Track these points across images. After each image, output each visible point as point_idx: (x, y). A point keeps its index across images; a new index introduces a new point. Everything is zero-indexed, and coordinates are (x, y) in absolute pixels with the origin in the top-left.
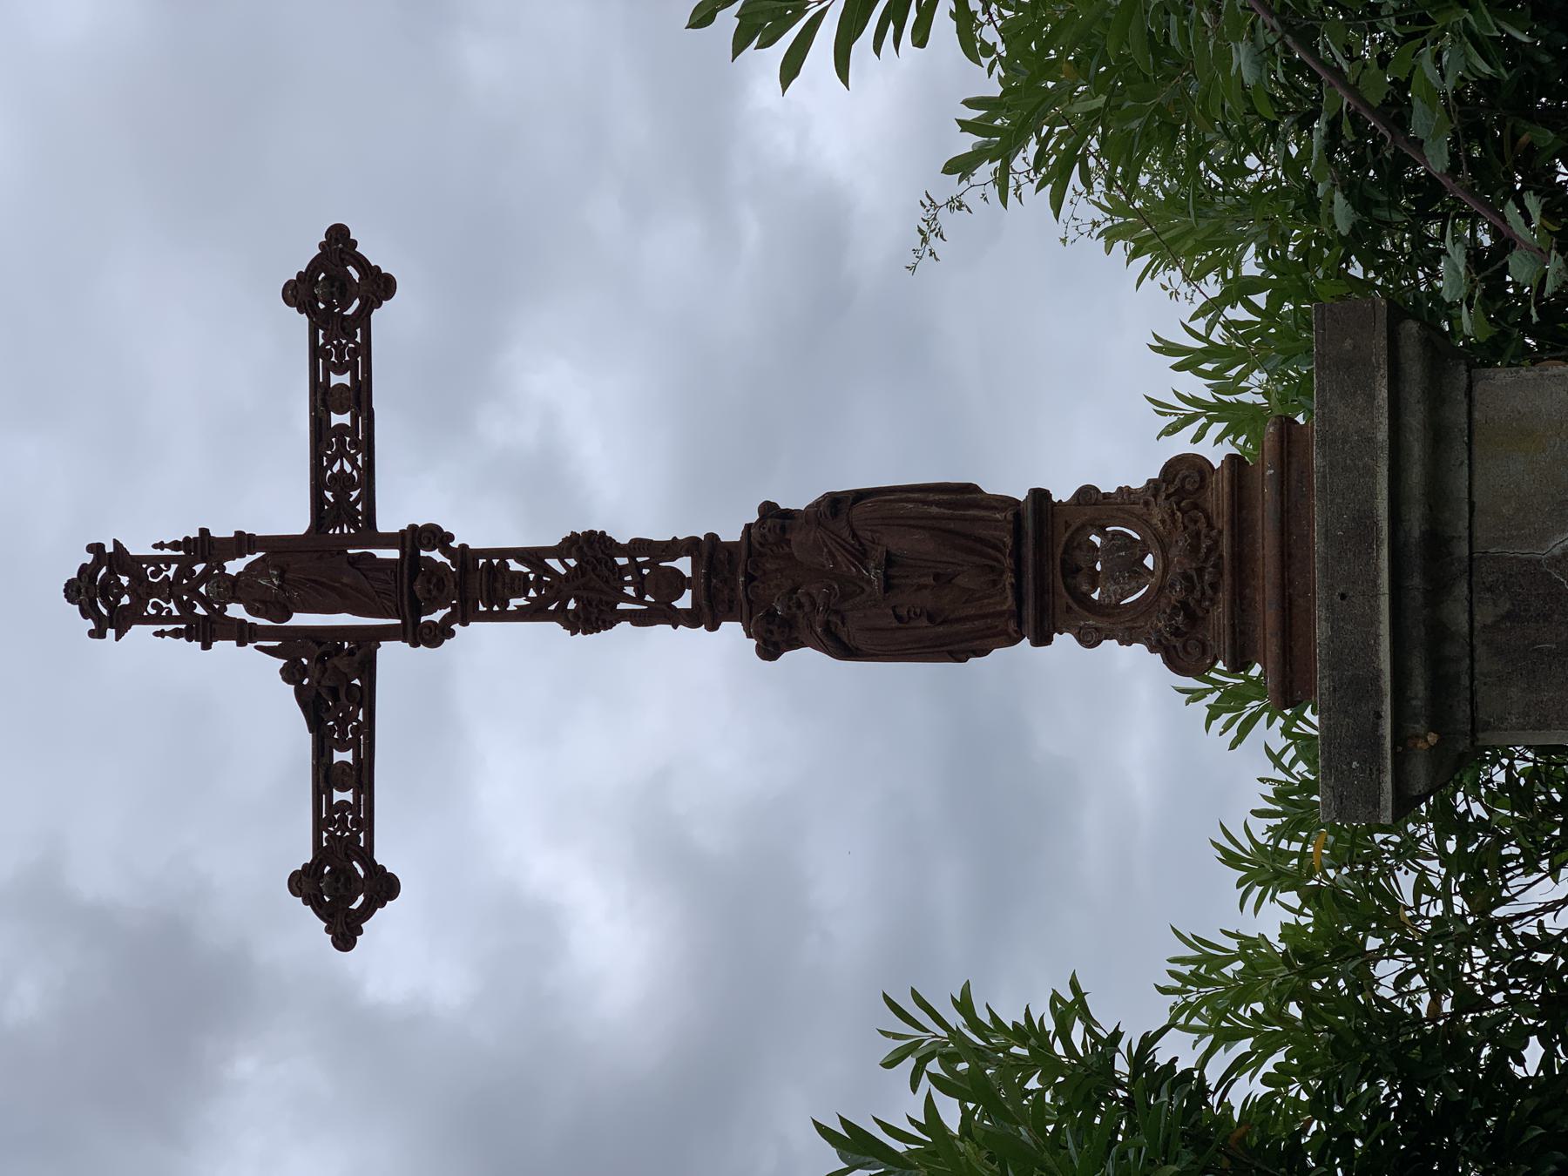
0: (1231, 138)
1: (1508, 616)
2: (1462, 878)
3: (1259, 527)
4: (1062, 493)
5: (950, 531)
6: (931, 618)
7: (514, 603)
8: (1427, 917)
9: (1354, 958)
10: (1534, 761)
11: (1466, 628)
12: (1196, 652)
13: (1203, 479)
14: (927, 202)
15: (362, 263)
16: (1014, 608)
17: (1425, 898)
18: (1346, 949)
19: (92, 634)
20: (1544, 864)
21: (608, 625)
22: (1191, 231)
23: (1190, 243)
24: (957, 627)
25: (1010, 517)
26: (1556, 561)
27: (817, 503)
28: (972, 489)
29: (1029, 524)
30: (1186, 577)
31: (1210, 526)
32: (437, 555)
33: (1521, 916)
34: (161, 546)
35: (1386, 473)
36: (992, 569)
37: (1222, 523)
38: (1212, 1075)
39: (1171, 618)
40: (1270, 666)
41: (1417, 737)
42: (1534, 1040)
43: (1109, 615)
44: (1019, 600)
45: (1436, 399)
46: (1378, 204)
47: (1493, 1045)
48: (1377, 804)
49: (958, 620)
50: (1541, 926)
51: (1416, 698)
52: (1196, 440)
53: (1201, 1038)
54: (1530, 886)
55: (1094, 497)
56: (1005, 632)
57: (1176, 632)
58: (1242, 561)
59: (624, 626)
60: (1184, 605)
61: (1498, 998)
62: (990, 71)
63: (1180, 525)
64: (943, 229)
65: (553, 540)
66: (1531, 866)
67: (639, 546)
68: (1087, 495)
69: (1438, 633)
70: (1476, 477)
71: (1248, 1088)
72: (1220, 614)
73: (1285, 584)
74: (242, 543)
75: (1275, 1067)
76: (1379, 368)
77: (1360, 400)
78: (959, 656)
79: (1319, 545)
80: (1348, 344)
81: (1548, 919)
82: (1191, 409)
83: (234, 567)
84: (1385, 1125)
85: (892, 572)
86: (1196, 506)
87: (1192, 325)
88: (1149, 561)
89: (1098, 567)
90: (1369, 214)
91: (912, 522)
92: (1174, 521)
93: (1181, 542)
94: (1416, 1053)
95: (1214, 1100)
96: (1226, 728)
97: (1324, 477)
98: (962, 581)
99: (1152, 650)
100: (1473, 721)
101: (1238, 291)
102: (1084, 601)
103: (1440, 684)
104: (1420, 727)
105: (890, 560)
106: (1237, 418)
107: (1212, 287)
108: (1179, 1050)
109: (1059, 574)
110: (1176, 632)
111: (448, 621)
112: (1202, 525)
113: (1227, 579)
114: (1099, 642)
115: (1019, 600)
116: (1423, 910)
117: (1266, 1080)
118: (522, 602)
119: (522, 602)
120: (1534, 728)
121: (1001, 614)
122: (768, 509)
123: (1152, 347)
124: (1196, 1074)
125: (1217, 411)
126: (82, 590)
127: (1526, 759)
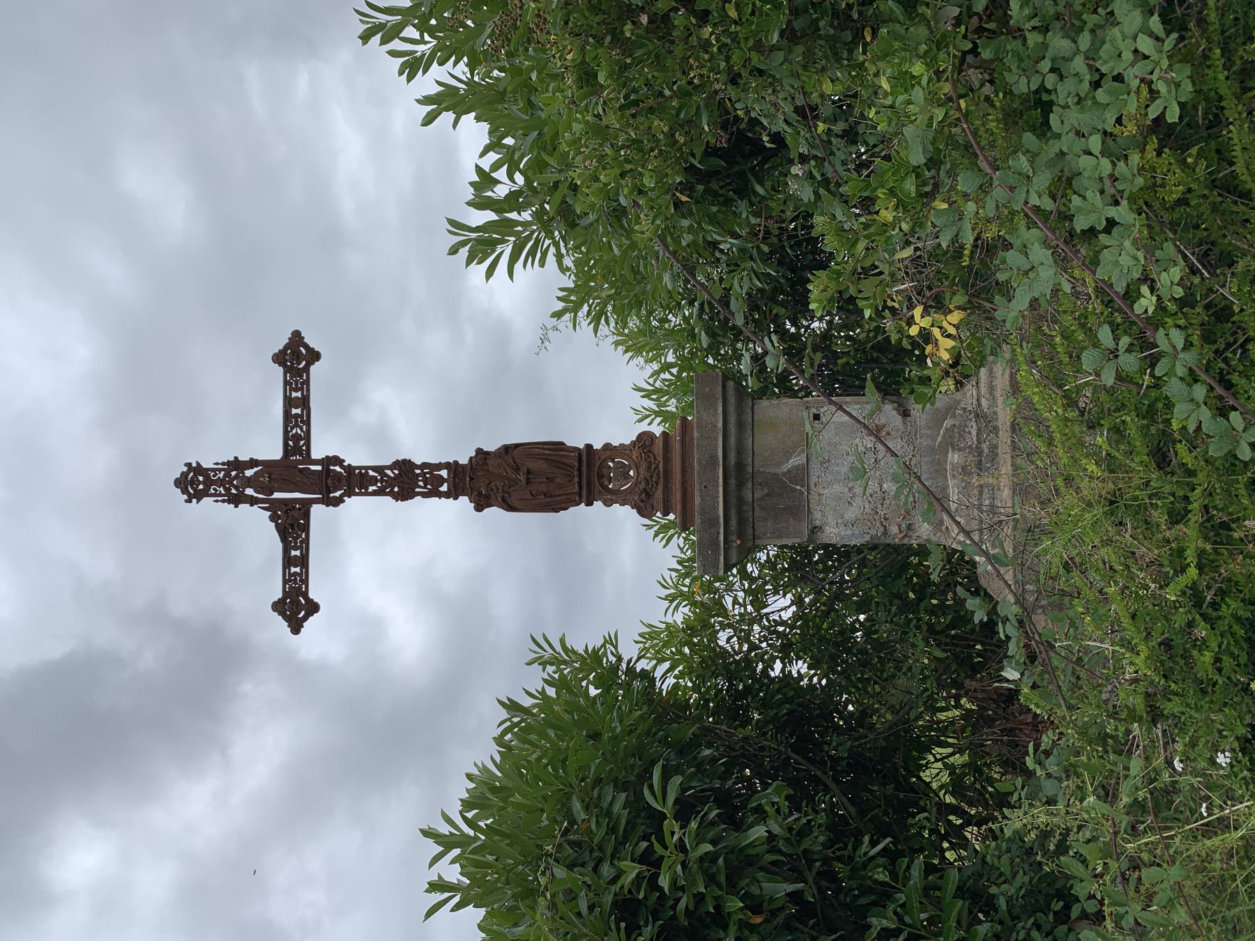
1: (767, 495)
4: (598, 446)
6: (545, 495)
7: (371, 489)
15: (306, 346)
19: (186, 501)
21: (412, 498)
24: (555, 499)
26: (784, 474)
27: (499, 449)
28: (562, 443)
29: (584, 458)
31: (655, 459)
32: (338, 469)
34: (217, 464)
37: (660, 458)
44: (580, 488)
46: (719, 335)
48: (718, 568)
50: (780, 616)
52: (649, 424)
58: (667, 473)
59: (418, 498)
60: (645, 490)
65: (389, 463)
66: (776, 593)
67: (425, 465)
68: (607, 447)
69: (741, 500)
72: (659, 494)
73: (684, 483)
74: (253, 463)
78: (556, 510)
80: (707, 389)
82: (648, 413)
83: (249, 473)
86: (650, 451)
88: (631, 473)
93: (644, 465)
96: (662, 539)
103: (741, 521)
104: (734, 538)
105: (529, 472)
111: (342, 496)
113: (662, 480)
115: (580, 488)
118: (375, 488)
119: (375, 488)
122: (479, 451)
126: (182, 483)
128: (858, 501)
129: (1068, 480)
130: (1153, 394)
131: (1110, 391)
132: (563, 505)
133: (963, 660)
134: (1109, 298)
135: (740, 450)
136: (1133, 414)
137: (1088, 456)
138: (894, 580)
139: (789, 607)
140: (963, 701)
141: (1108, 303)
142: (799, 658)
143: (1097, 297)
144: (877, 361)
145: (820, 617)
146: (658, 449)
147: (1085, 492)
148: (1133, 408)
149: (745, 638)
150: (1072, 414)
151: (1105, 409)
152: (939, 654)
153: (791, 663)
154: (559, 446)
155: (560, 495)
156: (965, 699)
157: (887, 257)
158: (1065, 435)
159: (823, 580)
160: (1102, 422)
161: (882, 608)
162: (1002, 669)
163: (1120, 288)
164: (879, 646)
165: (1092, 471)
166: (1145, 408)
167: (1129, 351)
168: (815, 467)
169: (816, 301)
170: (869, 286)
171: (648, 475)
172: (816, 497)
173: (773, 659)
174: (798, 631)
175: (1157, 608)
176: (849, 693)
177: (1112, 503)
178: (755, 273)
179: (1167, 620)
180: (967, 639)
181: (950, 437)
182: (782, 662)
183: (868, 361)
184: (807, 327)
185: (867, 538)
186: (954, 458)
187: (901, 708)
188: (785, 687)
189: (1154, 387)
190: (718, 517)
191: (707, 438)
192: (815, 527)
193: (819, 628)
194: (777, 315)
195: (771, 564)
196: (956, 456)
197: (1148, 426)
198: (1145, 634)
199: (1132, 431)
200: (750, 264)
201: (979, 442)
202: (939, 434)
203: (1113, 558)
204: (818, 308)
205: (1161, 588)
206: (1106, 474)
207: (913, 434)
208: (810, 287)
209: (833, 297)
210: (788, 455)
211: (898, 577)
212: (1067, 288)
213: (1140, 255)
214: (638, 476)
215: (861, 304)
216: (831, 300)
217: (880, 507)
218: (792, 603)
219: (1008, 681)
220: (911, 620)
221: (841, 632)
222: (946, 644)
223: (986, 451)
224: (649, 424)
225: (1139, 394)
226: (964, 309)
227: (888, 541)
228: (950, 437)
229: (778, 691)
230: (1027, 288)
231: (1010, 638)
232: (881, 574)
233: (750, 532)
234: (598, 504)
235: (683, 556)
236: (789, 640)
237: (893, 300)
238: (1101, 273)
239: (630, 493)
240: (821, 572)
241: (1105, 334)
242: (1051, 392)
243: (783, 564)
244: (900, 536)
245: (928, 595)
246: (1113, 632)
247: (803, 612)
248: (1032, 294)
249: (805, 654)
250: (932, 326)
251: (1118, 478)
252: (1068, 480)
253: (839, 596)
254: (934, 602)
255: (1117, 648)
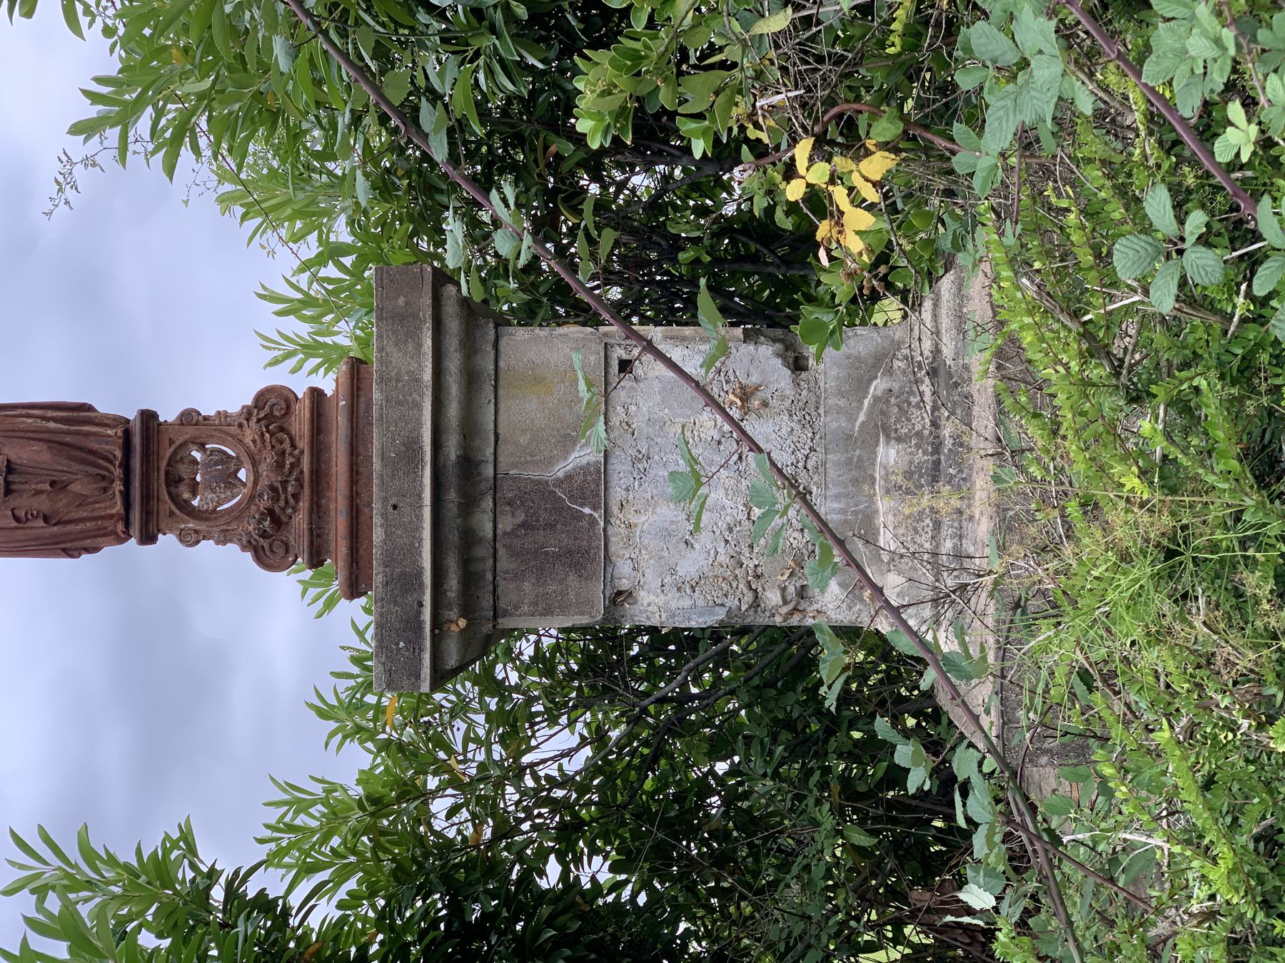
0: (322, 128)
1: (523, 525)
2: (501, 731)
3: (333, 449)
4: (168, 414)
5: (67, 444)
6: (46, 519)
8: (473, 761)
9: (415, 799)
10: (557, 638)
11: (491, 535)
12: (281, 551)
13: (288, 407)
14: (64, 159)
16: (122, 511)
17: (472, 746)
18: (409, 792)
20: (564, 720)
22: (289, 201)
23: (289, 211)
24: (69, 528)
25: (120, 433)
26: (559, 482)
28: (90, 408)
29: (137, 440)
30: (272, 488)
31: (294, 446)
33: (544, 761)
35: (429, 407)
36: (104, 477)
37: (304, 444)
38: (295, 900)
39: (259, 522)
40: (341, 563)
41: (451, 622)
42: (552, 857)
43: (206, 520)
44: (127, 505)
45: (470, 348)
46: (441, 191)
47: (521, 864)
48: (418, 677)
49: (70, 522)
50: (560, 769)
51: (451, 591)
52: (294, 371)
53: (288, 872)
54: (552, 736)
55: (195, 418)
56: (114, 533)
57: (264, 535)
58: (319, 477)
60: (270, 512)
61: (526, 826)
62: (112, 51)
63: (268, 444)
64: (78, 182)
66: (553, 721)
68: (189, 418)
69: (469, 538)
70: (501, 411)
71: (324, 913)
72: (300, 520)
75: (348, 893)
76: (425, 321)
77: (410, 347)
78: (69, 553)
79: (377, 465)
80: (401, 301)
81: (565, 761)
82: (292, 347)
84: (436, 933)
85: (11, 478)
86: (282, 429)
87: (294, 280)
88: (242, 474)
89: (198, 478)
90: (432, 199)
91: (31, 435)
92: (263, 442)
93: (269, 458)
94: (461, 874)
95: (294, 922)
97: (381, 409)
98: (76, 487)
99: (244, 548)
100: (495, 608)
101: (333, 252)
102: (185, 507)
103: (470, 579)
104: (453, 614)
106: (329, 355)
107: (310, 247)
108: (271, 882)
109: (163, 485)
110: (264, 535)
112: (287, 445)
113: (307, 490)
114: (197, 542)
115: (127, 505)
116: (470, 755)
117: (340, 906)
120: (541, 615)
121: (111, 516)
123: (258, 295)
124: (280, 902)
125: (310, 349)
127: (551, 636)
128: (704, 540)
129: (1091, 507)
130: (1252, 333)
131: (1172, 326)
132: (88, 543)
133: (907, 850)
134: (1173, 135)
135: (469, 429)
136: (1213, 374)
137: (1126, 457)
138: (781, 693)
139: (577, 749)
140: (908, 930)
141: (1172, 146)
142: (594, 851)
143: (1151, 133)
144: (755, 258)
145: (638, 769)
146: (300, 423)
147: (1119, 533)
148: (1213, 362)
149: (488, 807)
150: (1098, 371)
151: (1163, 363)
152: (861, 839)
153: (578, 861)
154: (79, 413)
155: (83, 520)
156: (911, 927)
157: (737, 27)
158: (1083, 414)
159: (646, 694)
160: (1154, 389)
161: (755, 748)
162: (961, 883)
163: (1189, 108)
164: (750, 823)
165: (1132, 490)
166: (1236, 363)
167: (1204, 240)
168: (621, 470)
169: (591, 116)
170: (698, 92)
171: (276, 479)
172: (623, 530)
173: (542, 855)
174: (595, 798)
175: (1252, 768)
176: (692, 919)
177: (1170, 554)
178: (502, 62)
179: (1271, 791)
180: (915, 809)
181: (883, 413)
182: (561, 860)
183: (738, 259)
184: (621, 186)
185: (721, 614)
186: (889, 455)
187: (789, 949)
188: (563, 912)
189: (1254, 320)
190: (420, 574)
191: (399, 403)
192: (620, 593)
193: (634, 790)
194: (559, 157)
195: (542, 662)
196: (892, 452)
197: (1241, 400)
198: (1229, 820)
199: (1211, 408)
200: (489, 41)
201: (935, 424)
202: (860, 408)
203: (1171, 665)
204: (594, 130)
205: (1260, 727)
206: (1158, 496)
207: (811, 406)
208: (580, 85)
209: (623, 109)
210: (568, 441)
211: (790, 687)
212: (1086, 105)
213: (1228, 35)
214: (256, 483)
215: (686, 126)
216: (621, 113)
217: (746, 551)
218: (584, 742)
219: (970, 911)
220: (810, 773)
221: (680, 798)
222: (876, 819)
223: (948, 443)
224: (294, 371)
225: (1226, 332)
226: (896, 150)
227: (767, 622)
228: (883, 413)
229: (550, 922)
230: (1009, 103)
231: (977, 825)
232: (756, 681)
233: (487, 602)
234: (167, 541)
235: (363, 647)
236: (575, 815)
237: (757, 126)
238: (1152, 72)
239: (239, 518)
240: (640, 679)
241: (1158, 204)
242: (1056, 326)
243: (567, 664)
244: (784, 610)
245: (845, 727)
246: (1171, 814)
247: (604, 759)
248: (1020, 118)
249: (608, 842)
250: (832, 181)
251: (1180, 504)
252: (1091, 507)
253: (679, 727)
254: (856, 735)
255: (1177, 849)
